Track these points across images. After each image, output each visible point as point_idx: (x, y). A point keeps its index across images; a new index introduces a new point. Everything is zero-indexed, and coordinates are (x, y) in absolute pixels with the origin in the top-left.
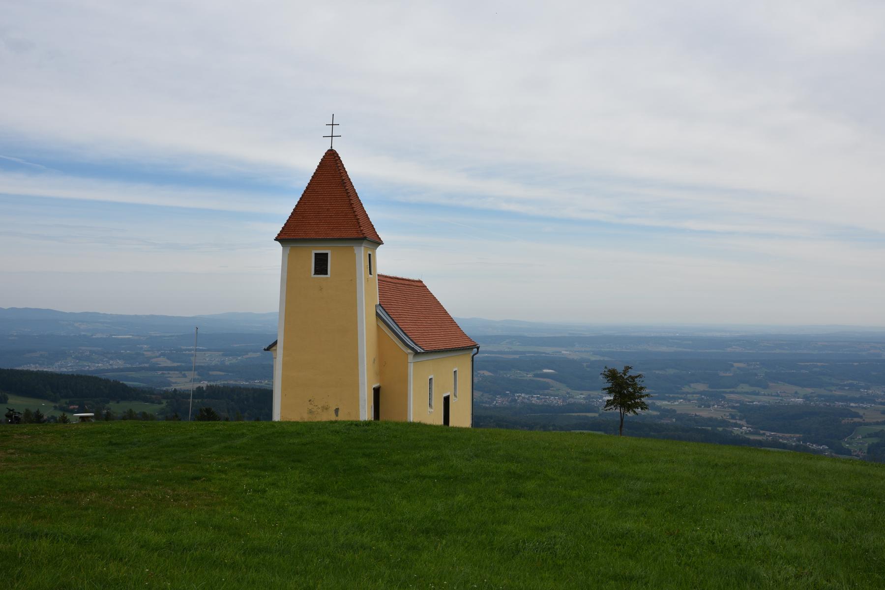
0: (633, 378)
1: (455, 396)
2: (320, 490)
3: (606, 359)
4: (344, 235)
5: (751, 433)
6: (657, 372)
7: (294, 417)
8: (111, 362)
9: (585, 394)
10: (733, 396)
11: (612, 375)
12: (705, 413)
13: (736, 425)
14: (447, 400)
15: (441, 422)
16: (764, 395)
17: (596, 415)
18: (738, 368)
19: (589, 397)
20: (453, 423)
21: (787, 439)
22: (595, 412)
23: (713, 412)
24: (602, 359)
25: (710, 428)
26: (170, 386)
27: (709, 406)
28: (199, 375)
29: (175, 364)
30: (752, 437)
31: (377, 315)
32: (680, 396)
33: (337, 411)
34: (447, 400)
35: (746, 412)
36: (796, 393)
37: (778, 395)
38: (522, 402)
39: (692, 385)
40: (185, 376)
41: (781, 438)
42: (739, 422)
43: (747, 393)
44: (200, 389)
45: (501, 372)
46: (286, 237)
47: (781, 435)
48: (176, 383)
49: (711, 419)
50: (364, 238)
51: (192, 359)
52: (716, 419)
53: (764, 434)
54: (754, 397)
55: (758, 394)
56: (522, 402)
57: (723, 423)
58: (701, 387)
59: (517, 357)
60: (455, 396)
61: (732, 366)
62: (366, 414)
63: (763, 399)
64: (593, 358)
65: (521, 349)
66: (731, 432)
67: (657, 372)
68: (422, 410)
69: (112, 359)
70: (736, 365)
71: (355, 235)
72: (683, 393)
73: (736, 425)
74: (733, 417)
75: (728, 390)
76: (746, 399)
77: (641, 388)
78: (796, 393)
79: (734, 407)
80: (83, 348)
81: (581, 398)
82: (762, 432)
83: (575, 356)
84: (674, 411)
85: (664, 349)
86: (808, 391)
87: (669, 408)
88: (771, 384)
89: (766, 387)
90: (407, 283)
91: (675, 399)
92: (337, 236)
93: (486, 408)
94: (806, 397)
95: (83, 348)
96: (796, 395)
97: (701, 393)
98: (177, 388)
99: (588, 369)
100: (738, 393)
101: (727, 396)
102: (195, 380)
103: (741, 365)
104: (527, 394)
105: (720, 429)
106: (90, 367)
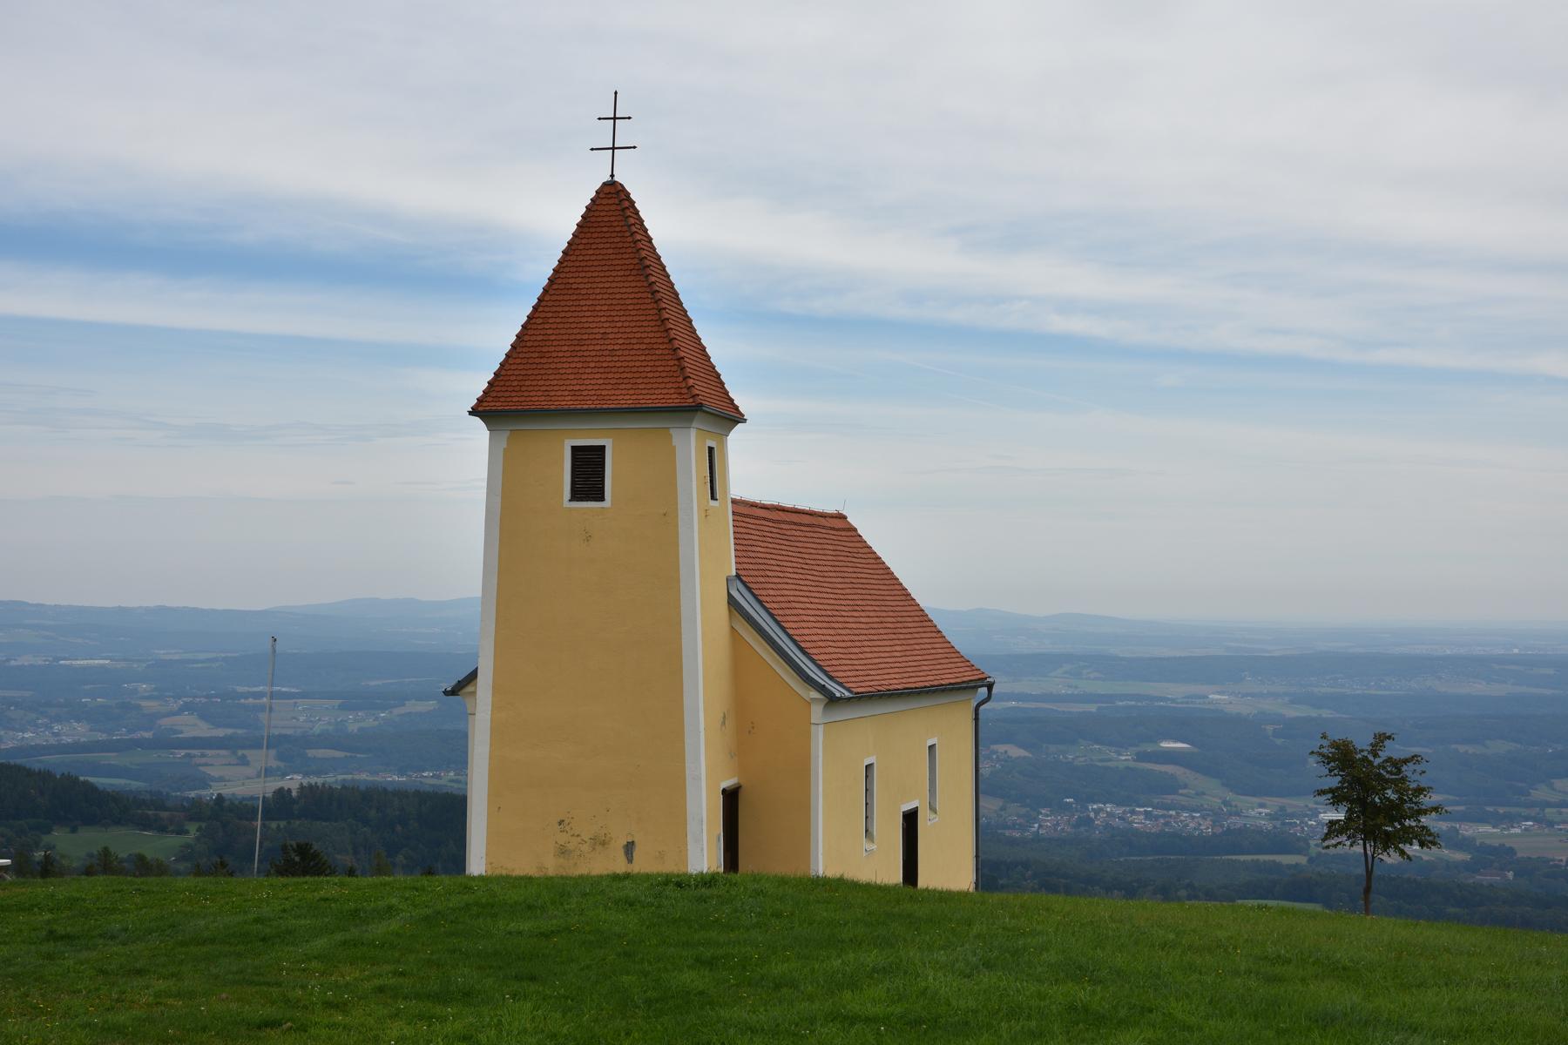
3: (1326, 713)
6: (1462, 749)
7: (523, 865)
8: (57, 728)
9: (1273, 804)
11: (1342, 757)
14: (911, 819)
15: (895, 876)
17: (1302, 860)
22: (1299, 852)
24: (1314, 713)
26: (206, 786)
31: (732, 601)
32: (1524, 811)
34: (911, 819)
40: (244, 762)
44: (281, 794)
46: (498, 406)
48: (221, 779)
51: (263, 716)
59: (1093, 708)
60: (933, 809)
62: (704, 856)
64: (1292, 713)
65: (1102, 688)
67: (1462, 749)
68: (845, 847)
69: (58, 719)
71: (674, 401)
77: (1419, 791)
84: (1511, 851)
85: (1479, 688)
87: (1496, 843)
91: (1512, 820)
99: (1279, 741)
102: (268, 772)
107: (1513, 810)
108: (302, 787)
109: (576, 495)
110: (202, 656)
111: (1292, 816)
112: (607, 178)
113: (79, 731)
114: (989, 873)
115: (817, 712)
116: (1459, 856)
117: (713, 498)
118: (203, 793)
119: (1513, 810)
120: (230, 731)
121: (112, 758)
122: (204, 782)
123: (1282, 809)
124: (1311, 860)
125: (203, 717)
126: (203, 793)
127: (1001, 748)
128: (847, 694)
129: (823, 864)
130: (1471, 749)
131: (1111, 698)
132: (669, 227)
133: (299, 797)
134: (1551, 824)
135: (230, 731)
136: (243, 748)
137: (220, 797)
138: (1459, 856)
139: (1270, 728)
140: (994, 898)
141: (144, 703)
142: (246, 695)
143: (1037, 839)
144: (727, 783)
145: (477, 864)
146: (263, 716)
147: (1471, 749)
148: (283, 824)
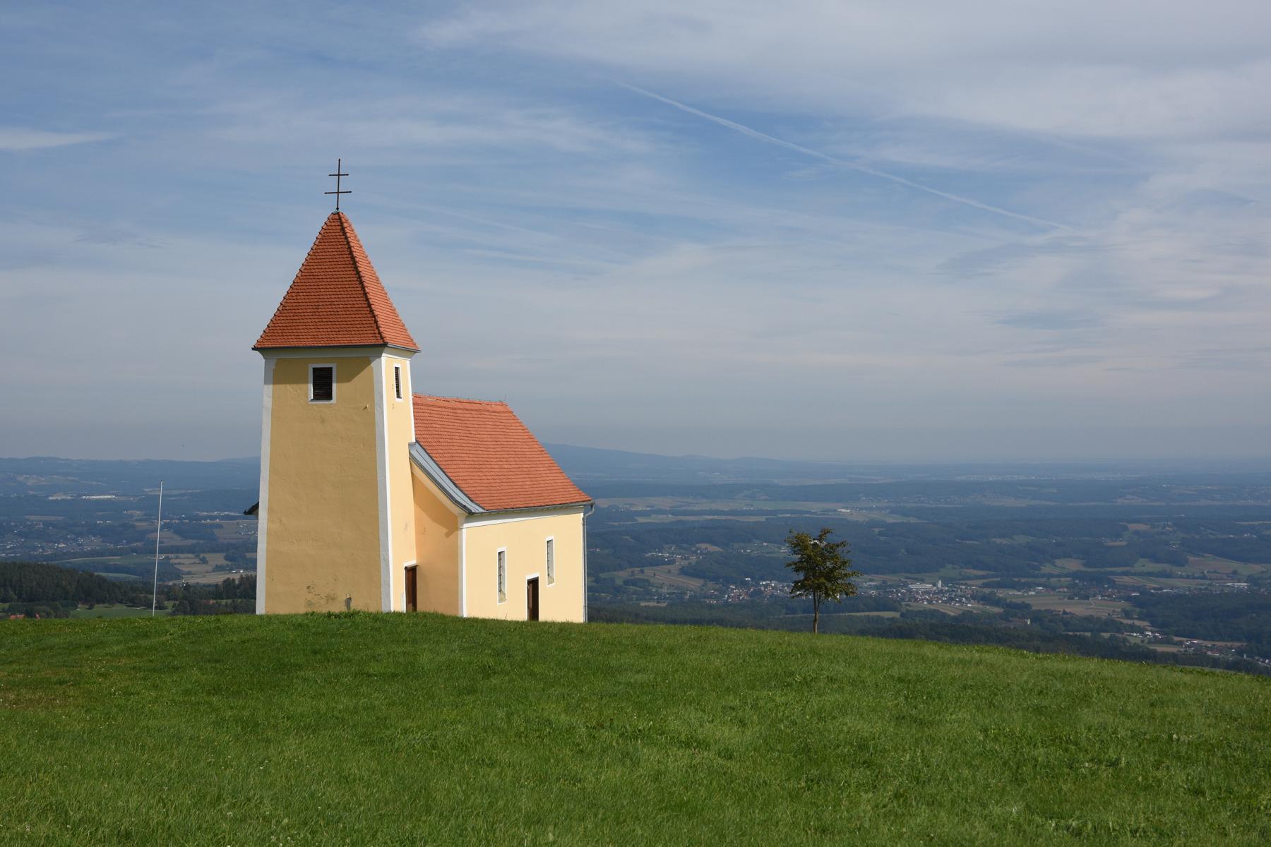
0: (832, 548)
1: (551, 580)
2: (216, 690)
3: (912, 520)
4: (356, 342)
5: (1156, 641)
6: (998, 541)
7: (283, 610)
8: (81, 541)
9: (877, 580)
10: (1126, 579)
11: (798, 544)
12: (1079, 609)
13: (1133, 628)
14: (533, 584)
15: (522, 614)
16: (1181, 577)
17: (897, 615)
18: (1136, 533)
19: (883, 587)
20: (543, 616)
21: (1220, 650)
22: (895, 610)
23: (1097, 607)
24: (905, 520)
25: (1088, 634)
26: (179, 577)
27: (1087, 598)
28: (227, 558)
29: (189, 542)
30: (1160, 649)
31: (412, 458)
32: (1037, 580)
33: (348, 601)
34: (533, 584)
35: (1147, 606)
36: (1235, 572)
37: (1204, 577)
38: (772, 595)
39: (1058, 562)
40: (204, 561)
41: (1211, 649)
42: (1137, 623)
43: (1150, 574)
44: (228, 583)
45: (736, 545)
46: (268, 344)
47: (1209, 644)
48: (189, 573)
49: (1089, 619)
50: (385, 345)
51: (216, 531)
52: (1099, 619)
53: (1181, 643)
54: (1161, 580)
55: (1169, 576)
56: (772, 595)
57: (1109, 624)
58: (1073, 565)
59: (763, 519)
60: (551, 580)
61: (1126, 529)
62: (397, 601)
63: (1180, 584)
64: (891, 520)
65: (769, 506)
66: (1125, 640)
67: (998, 541)
68: (485, 597)
69: (81, 535)
70: (1133, 527)
71: (373, 342)
72: (1043, 576)
73: (1133, 628)
74: (1127, 615)
75: (1119, 570)
76: (1151, 585)
77: (844, 563)
78: (1235, 572)
79: (1129, 599)
80: (32, 518)
81: (871, 588)
82: (1176, 639)
83: (860, 517)
84: (1028, 606)
85: (1010, 502)
86: (1257, 569)
87: (1019, 601)
88: (1191, 558)
89: (1180, 563)
90: (476, 407)
91: (1030, 586)
92: (344, 342)
93: (711, 607)
94: (1250, 579)
95: (32, 518)
96: (1234, 575)
97: (1075, 575)
98: (192, 581)
99: (882, 538)
100: (1135, 574)
101: (1117, 579)
102: (219, 568)
103: (1141, 527)
104: (780, 581)
105: (1106, 635)
106: (42, 550)
107: (1030, 580)
108: (242, 578)
109: (317, 397)
110: (176, 492)
111: (891, 586)
112: (334, 210)
113: (94, 543)
114: (594, 611)
115: (461, 519)
116: (996, 610)
117: (398, 396)
118: (177, 582)
119: (1030, 580)
120: (194, 542)
121: (116, 560)
122: (178, 575)
123: (884, 582)
124: (902, 615)
125: (175, 532)
126: (177, 582)
127: (703, 546)
128: (481, 510)
129: (469, 609)
130: (1005, 541)
131: (774, 512)
132: (369, 239)
133: (240, 584)
134: (1054, 588)
135: (194, 542)
136: (204, 552)
137: (188, 587)
138: (996, 610)
139: (877, 530)
140: (594, 625)
141: (137, 524)
142: (205, 518)
143: (727, 604)
144: (412, 562)
145: (261, 609)
146: (216, 531)
147: (1005, 541)
148: (229, 601)
